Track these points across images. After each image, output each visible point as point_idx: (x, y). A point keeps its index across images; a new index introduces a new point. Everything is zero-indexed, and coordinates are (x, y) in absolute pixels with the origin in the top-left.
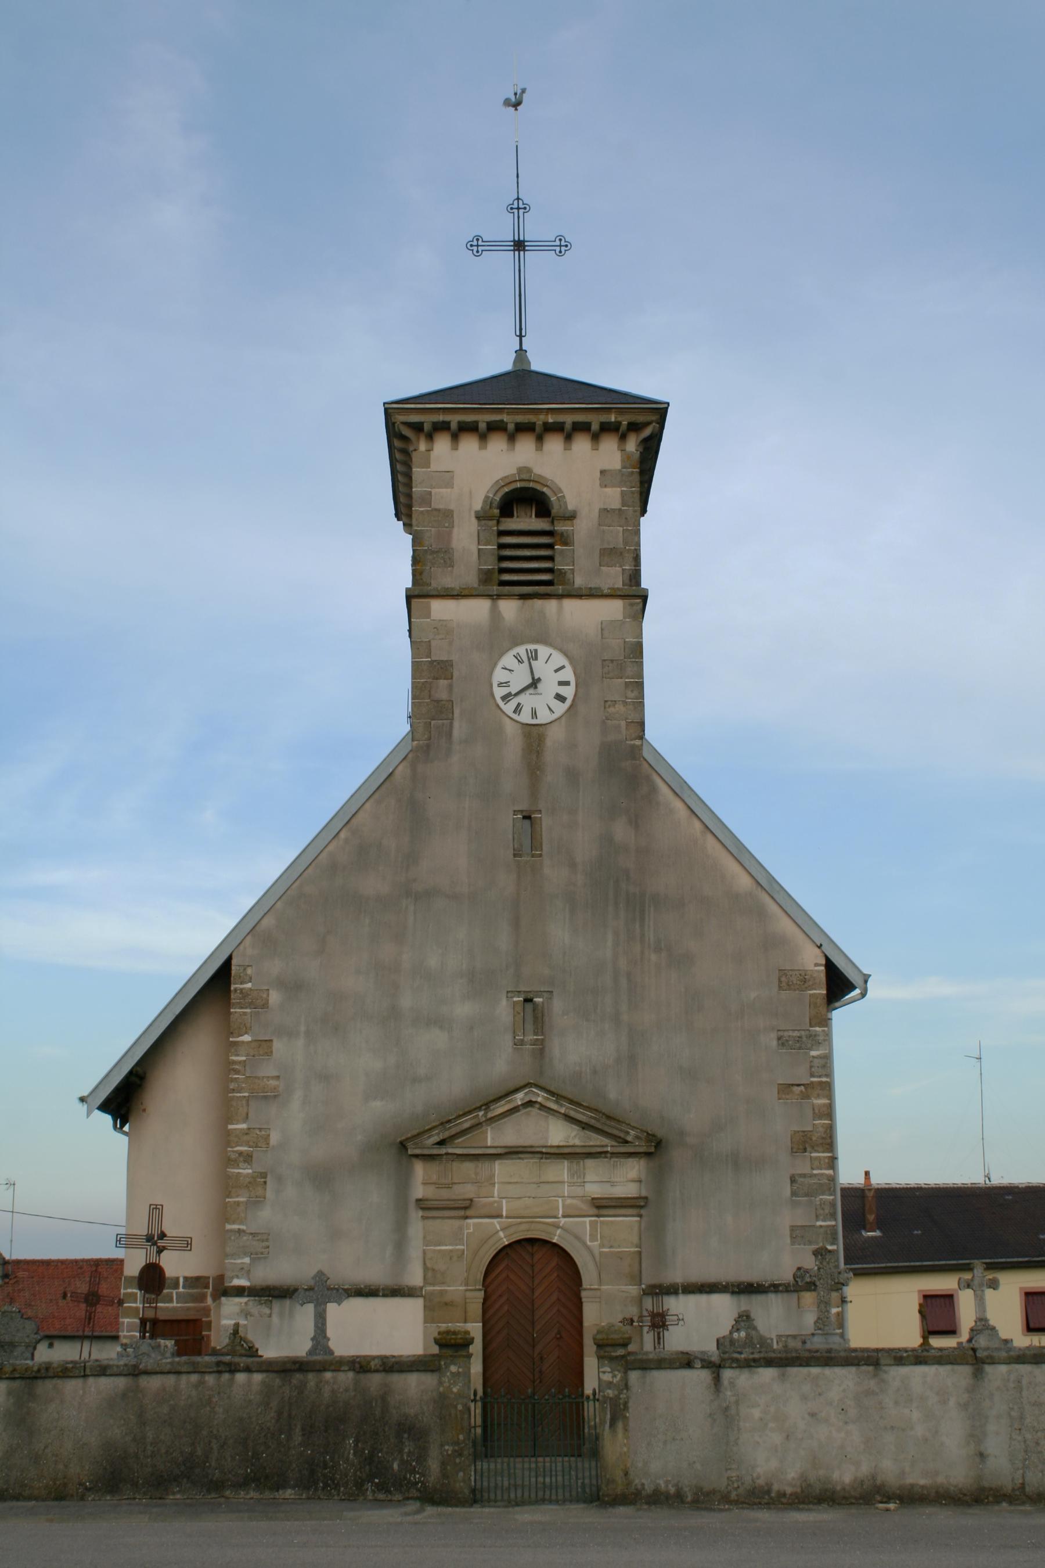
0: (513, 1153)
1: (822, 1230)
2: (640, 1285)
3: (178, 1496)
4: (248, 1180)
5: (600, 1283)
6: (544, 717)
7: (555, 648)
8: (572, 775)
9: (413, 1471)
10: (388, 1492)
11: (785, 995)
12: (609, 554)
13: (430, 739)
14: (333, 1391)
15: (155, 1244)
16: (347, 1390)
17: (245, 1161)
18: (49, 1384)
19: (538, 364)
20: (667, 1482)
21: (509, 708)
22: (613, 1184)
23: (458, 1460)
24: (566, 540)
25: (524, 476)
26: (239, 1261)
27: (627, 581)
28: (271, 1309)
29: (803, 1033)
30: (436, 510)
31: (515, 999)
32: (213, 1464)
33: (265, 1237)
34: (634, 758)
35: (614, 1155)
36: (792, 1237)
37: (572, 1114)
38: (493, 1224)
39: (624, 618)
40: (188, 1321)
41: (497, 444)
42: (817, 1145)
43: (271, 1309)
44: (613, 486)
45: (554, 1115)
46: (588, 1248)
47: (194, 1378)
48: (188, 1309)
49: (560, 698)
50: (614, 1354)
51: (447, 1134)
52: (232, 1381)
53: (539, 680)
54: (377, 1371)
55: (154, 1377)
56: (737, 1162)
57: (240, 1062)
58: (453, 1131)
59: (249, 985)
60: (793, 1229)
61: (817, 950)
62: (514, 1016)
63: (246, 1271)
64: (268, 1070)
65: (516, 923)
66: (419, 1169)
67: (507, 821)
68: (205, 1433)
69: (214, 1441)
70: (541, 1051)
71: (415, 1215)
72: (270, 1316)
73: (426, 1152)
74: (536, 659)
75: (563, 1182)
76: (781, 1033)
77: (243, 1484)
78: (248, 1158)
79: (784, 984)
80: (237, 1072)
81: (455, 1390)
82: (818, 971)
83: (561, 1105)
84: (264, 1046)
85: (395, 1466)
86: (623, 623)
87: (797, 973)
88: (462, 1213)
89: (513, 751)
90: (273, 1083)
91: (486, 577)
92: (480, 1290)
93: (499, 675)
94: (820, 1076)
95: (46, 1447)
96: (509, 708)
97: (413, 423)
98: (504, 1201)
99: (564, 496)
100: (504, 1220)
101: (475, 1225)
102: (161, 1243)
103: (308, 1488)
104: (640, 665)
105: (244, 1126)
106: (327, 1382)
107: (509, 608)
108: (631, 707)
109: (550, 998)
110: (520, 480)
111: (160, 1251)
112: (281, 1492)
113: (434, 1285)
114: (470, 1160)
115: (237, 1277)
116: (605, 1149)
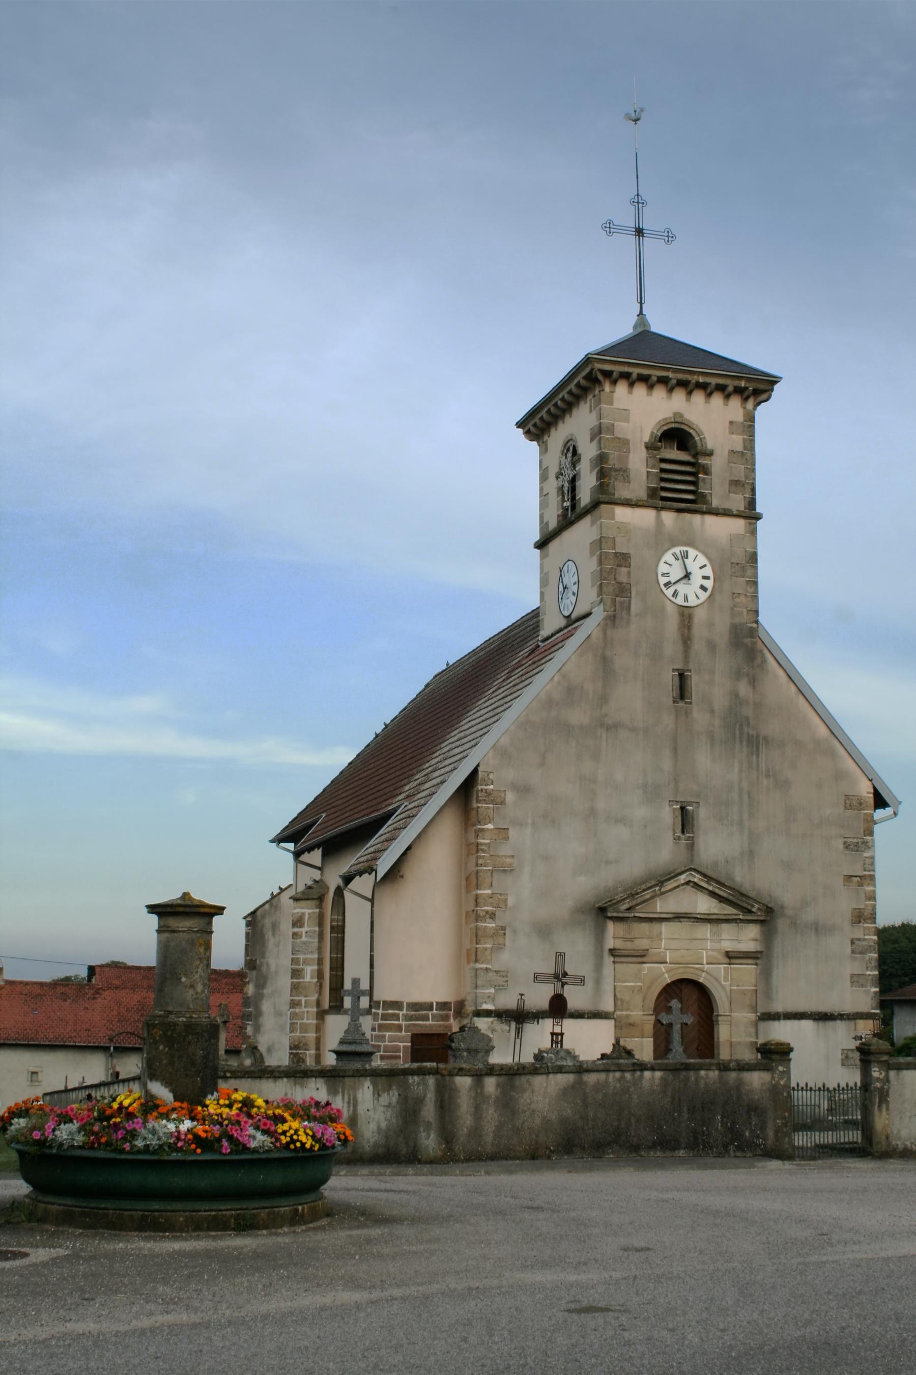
0: (678, 917)
1: (870, 977)
2: (756, 1013)
3: (611, 1156)
4: (492, 932)
5: (731, 1011)
6: (693, 601)
7: (700, 551)
8: (712, 646)
9: (758, 1137)
10: (743, 1151)
11: (848, 813)
12: (735, 484)
13: (615, 611)
14: (706, 1084)
15: (560, 980)
16: (714, 1082)
17: (490, 918)
18: (524, 1079)
19: (658, 326)
20: (912, 1143)
21: (669, 592)
22: (739, 941)
23: (785, 1130)
24: (707, 471)
25: (678, 420)
26: (487, 991)
27: (747, 505)
28: (510, 1027)
29: (859, 840)
30: (617, 438)
31: (675, 807)
32: (633, 1133)
33: (504, 974)
34: (752, 636)
35: (742, 921)
36: (852, 982)
37: (717, 891)
38: (660, 967)
39: (746, 533)
40: (439, 1035)
41: (660, 393)
42: (868, 918)
43: (510, 1027)
44: (738, 434)
45: (702, 891)
46: (722, 986)
47: (618, 1075)
48: (440, 1026)
49: (703, 588)
50: (881, 1059)
51: (634, 902)
52: (642, 1077)
53: (690, 573)
54: (734, 1070)
55: (592, 1074)
56: (817, 928)
57: (485, 844)
58: (639, 900)
59: (491, 787)
60: (852, 976)
61: (869, 783)
62: (674, 819)
63: (492, 998)
64: (504, 850)
65: (675, 750)
66: (611, 926)
67: (669, 678)
68: (626, 1112)
69: (632, 1118)
70: (691, 846)
71: (608, 960)
72: (509, 1031)
73: (621, 915)
74: (687, 558)
75: (707, 939)
76: (845, 840)
77: (653, 1146)
78: (493, 916)
79: (847, 805)
80: (483, 851)
81: (782, 1083)
82: (869, 797)
83: (710, 885)
84: (503, 832)
85: (747, 1134)
86: (744, 536)
87: (856, 798)
88: (640, 959)
89: (672, 624)
90: (509, 860)
91: (653, 493)
92: (652, 1015)
93: (662, 568)
94: (869, 871)
95: (523, 1123)
96: (669, 592)
97: (605, 371)
98: (668, 952)
99: (704, 438)
100: (668, 965)
101: (648, 968)
102: (564, 980)
103: (693, 1149)
104: (756, 568)
105: (489, 892)
106: (703, 1077)
107: (668, 517)
108: (750, 599)
109: (698, 807)
110: (675, 422)
111: (563, 985)
112: (676, 1152)
113: (622, 1010)
114: (646, 922)
115: (486, 1003)
116: (738, 917)
